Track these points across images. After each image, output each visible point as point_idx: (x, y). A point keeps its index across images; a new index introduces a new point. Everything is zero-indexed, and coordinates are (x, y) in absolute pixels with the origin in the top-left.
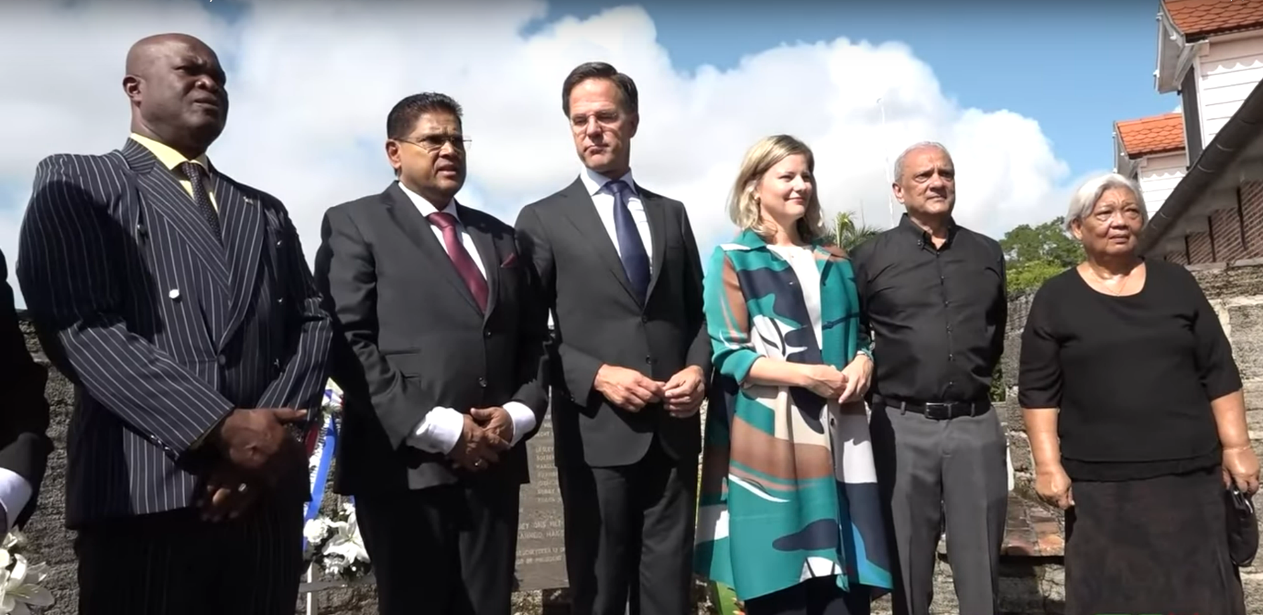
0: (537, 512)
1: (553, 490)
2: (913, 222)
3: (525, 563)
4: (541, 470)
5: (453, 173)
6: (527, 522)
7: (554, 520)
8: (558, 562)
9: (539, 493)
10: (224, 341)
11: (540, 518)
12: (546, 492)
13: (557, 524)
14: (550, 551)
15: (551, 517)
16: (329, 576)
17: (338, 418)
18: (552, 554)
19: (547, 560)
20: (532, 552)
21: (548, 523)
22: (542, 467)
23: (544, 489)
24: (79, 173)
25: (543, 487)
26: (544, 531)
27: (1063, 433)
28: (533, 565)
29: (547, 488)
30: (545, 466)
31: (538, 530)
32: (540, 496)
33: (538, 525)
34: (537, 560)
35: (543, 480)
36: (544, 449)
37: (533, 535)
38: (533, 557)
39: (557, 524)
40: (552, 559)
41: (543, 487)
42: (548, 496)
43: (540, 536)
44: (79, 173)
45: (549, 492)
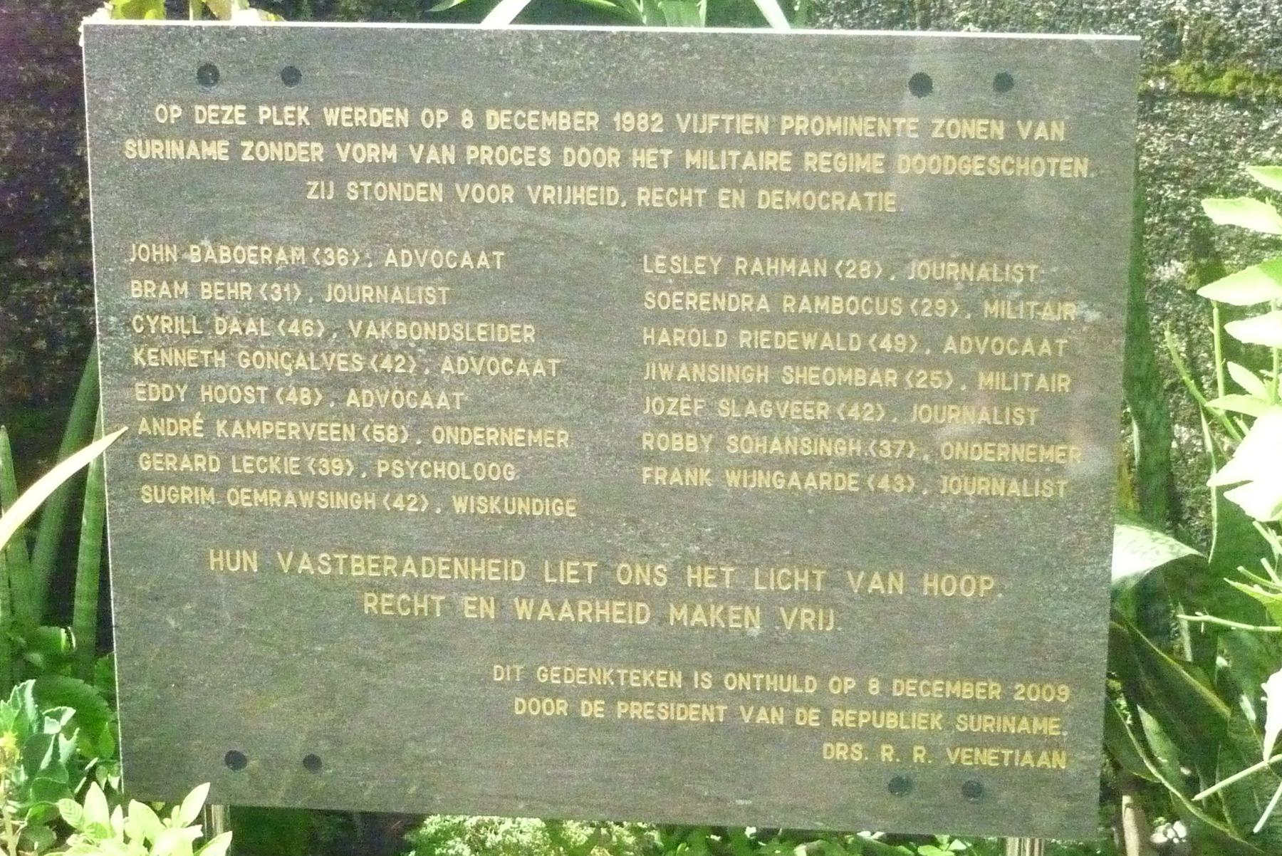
1: (707, 441)
2: (60, 634)
4: (665, 349)
6: (591, 554)
7: (705, 561)
9: (647, 444)
10: (1169, 665)
12: (677, 443)
15: (694, 549)
19: (667, 712)
20: (602, 676)
22: (664, 339)
24: (932, 584)
25: (664, 424)
26: (658, 599)
28: (606, 726)
29: (682, 426)
31: (632, 593)
32: (652, 458)
34: (621, 708)
37: (613, 612)
38: (611, 696)
39: (720, 577)
41: (664, 424)
42: (687, 460)
43: (640, 614)
44: (932, 584)
45: (691, 445)
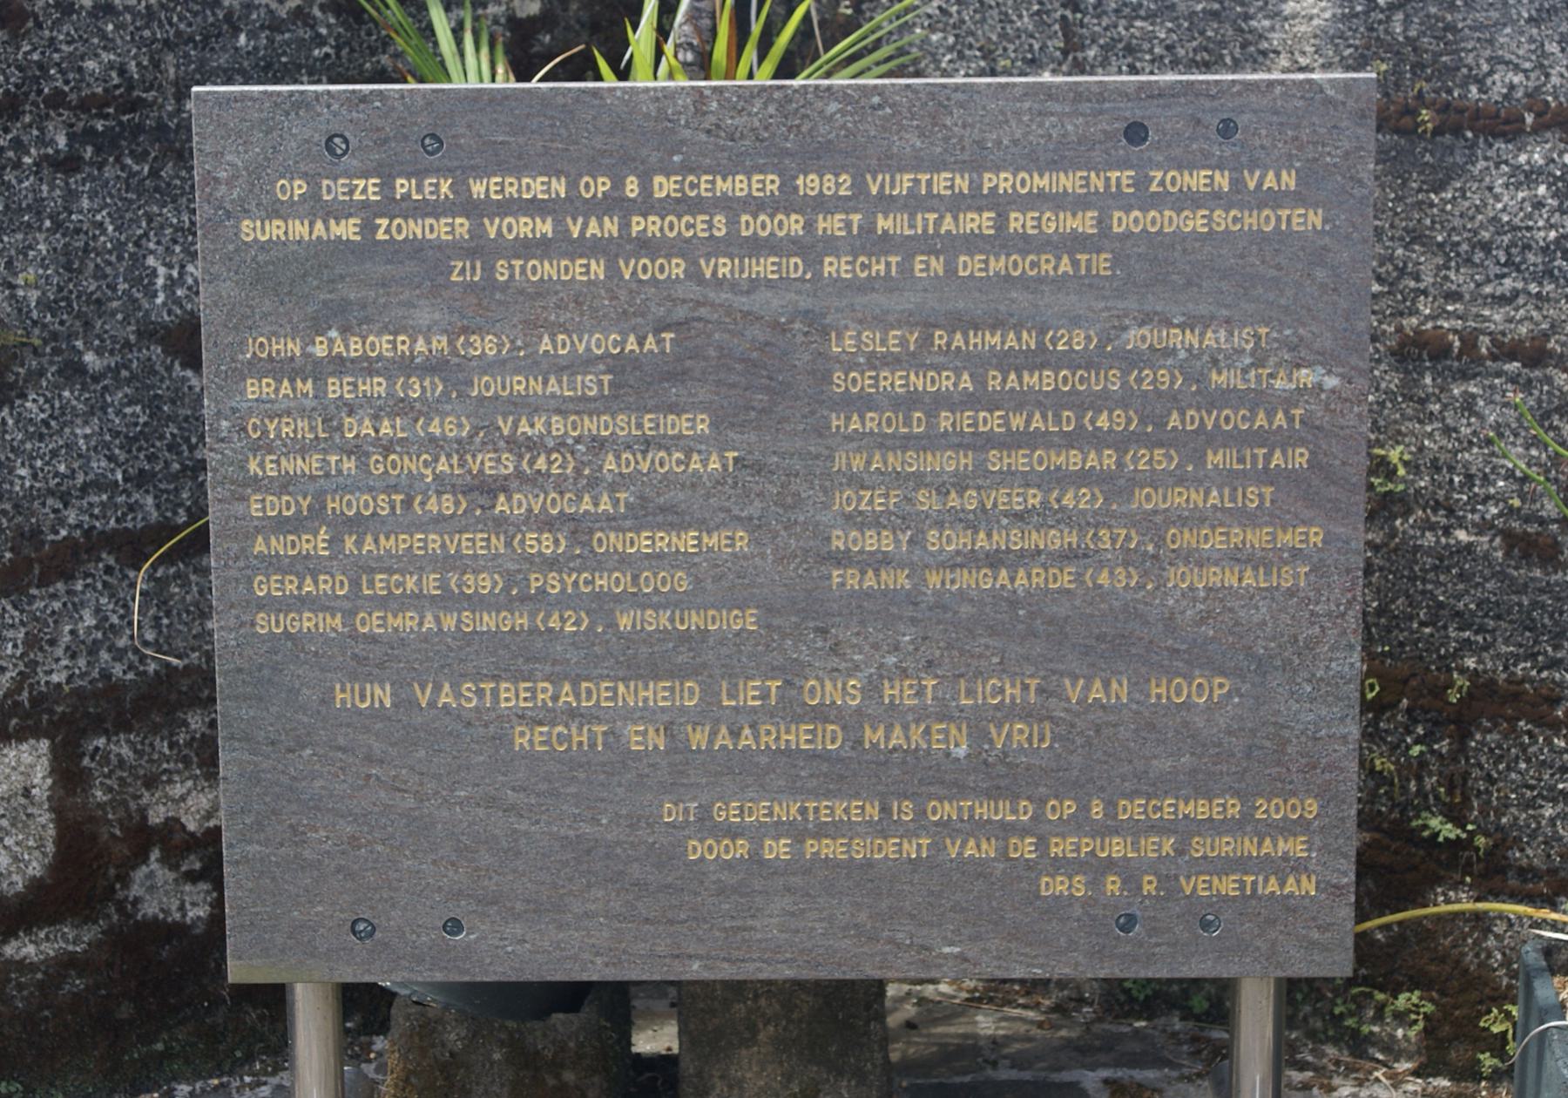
0: (823, 632)
1: (905, 538)
3: (755, 858)
5: (1261, 570)
6: (773, 672)
8: (914, 863)
11: (835, 662)
12: (871, 542)
13: (920, 693)
14: (873, 811)
15: (891, 660)
16: (1524, 101)
17: (1116, 262)
18: (882, 828)
19: (860, 850)
20: (787, 811)
21: (872, 689)
23: (861, 527)
26: (852, 722)
27: (199, 83)
28: (798, 866)
29: (875, 522)
30: (872, 421)
31: (820, 715)
32: (843, 559)
33: (822, 690)
35: (857, 482)
36: (871, 340)
37: (799, 737)
38: (797, 832)
39: (920, 693)
40: (889, 849)
42: (881, 561)
43: (832, 739)
